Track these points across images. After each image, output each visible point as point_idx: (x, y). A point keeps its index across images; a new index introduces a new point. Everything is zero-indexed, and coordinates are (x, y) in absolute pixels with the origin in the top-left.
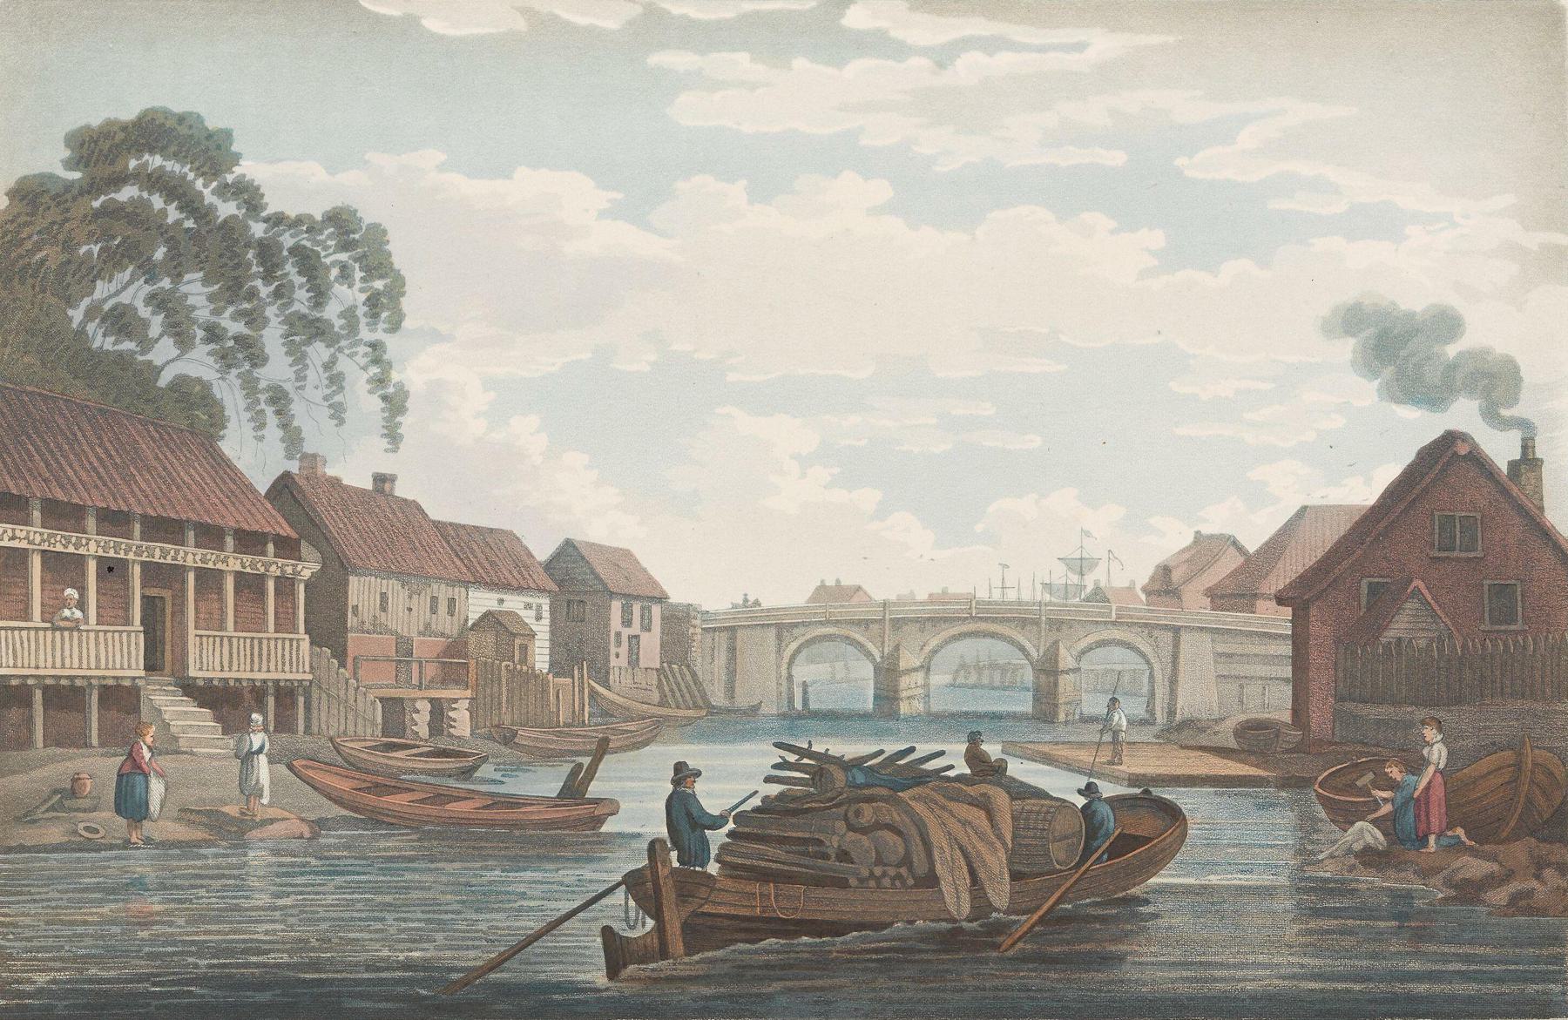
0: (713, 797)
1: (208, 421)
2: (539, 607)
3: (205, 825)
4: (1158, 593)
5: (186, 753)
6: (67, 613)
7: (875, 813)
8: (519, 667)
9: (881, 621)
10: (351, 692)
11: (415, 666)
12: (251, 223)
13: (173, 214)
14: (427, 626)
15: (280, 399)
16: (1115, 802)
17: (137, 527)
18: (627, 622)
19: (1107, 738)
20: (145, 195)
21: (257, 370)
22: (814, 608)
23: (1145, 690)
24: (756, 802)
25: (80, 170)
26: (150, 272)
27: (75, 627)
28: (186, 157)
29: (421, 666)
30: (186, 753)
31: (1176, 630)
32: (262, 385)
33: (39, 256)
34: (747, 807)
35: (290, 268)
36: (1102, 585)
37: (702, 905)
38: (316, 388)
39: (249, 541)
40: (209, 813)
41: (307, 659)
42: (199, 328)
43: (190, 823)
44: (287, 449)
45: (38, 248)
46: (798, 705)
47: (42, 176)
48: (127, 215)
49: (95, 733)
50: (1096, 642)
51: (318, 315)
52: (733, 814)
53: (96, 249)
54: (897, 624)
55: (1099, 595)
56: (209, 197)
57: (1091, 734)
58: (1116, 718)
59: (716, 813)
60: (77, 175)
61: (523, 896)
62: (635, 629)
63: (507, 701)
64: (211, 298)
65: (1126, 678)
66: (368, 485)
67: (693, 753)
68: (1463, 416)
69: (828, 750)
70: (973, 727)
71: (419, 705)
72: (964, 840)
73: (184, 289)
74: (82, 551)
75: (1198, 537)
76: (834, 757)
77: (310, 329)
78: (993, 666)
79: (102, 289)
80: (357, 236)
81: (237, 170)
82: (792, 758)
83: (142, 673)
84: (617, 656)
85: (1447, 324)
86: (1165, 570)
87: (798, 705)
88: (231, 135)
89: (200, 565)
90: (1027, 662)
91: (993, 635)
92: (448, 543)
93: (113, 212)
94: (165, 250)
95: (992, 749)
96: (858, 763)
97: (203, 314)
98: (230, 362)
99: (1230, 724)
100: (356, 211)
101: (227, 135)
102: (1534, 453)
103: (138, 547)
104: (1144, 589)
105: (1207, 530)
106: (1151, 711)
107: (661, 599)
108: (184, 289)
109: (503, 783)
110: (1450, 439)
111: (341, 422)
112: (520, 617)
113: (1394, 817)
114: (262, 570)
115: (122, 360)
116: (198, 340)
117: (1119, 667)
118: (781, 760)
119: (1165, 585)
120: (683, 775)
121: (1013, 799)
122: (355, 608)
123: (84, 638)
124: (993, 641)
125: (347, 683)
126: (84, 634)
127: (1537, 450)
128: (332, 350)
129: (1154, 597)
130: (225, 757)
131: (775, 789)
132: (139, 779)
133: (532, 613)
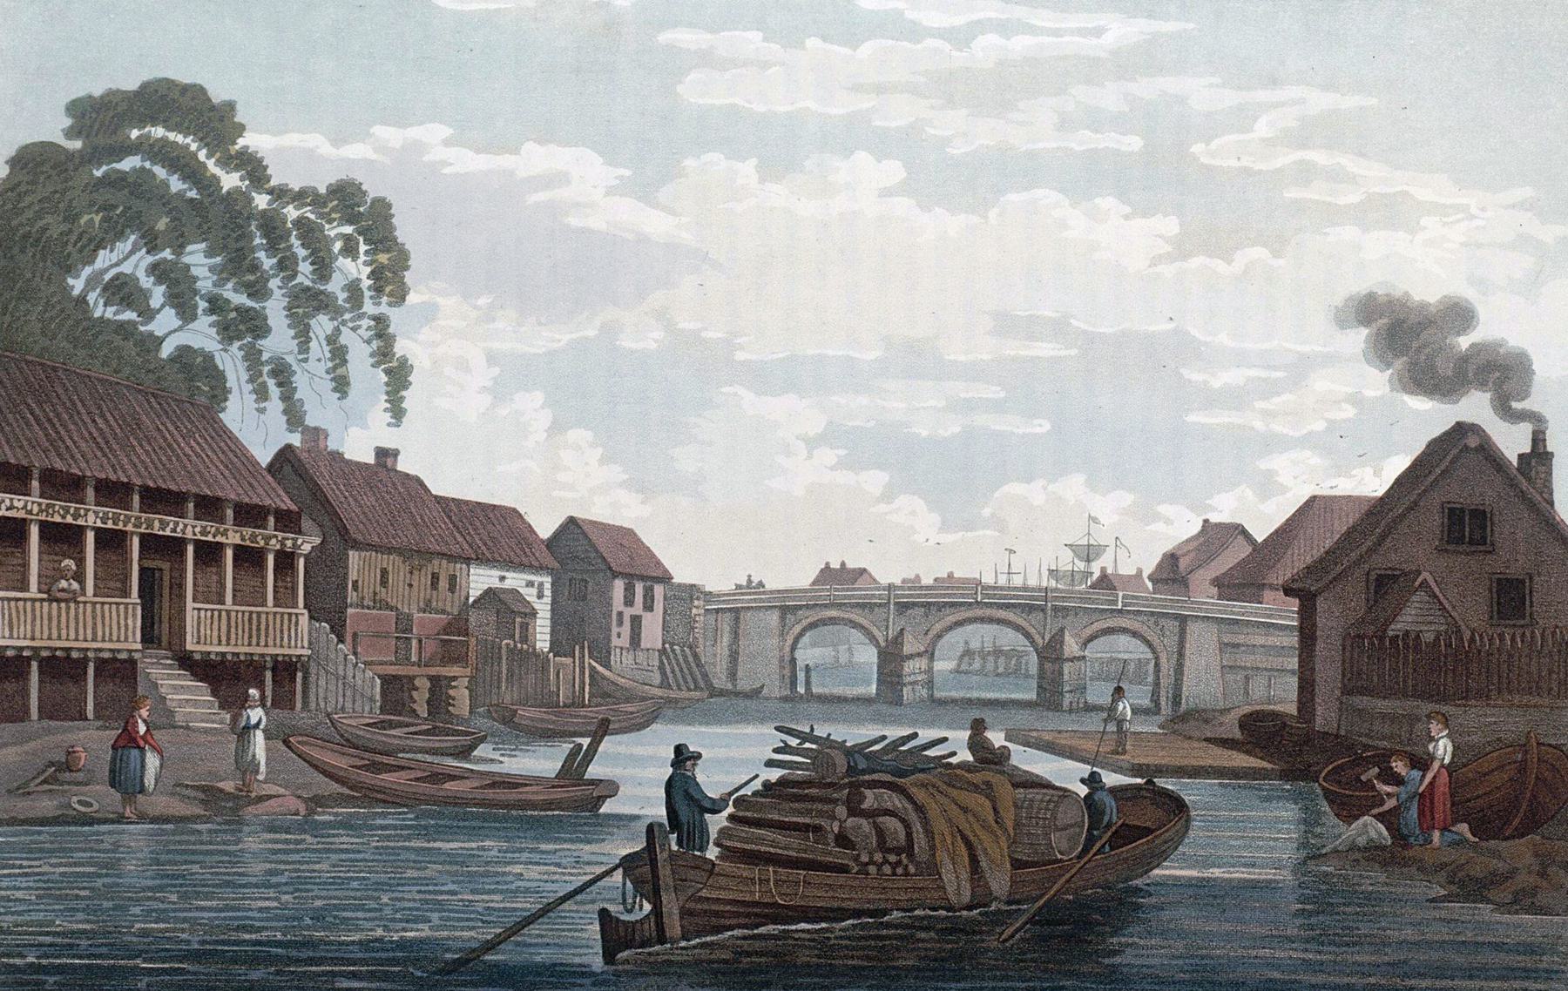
0: (712, 780)
2: (541, 585)
4: (1166, 581)
6: (63, 584)
8: (519, 645)
10: (350, 666)
11: (414, 643)
13: (176, 184)
14: (428, 602)
17: (136, 498)
18: (629, 602)
19: (1112, 727)
20: (147, 165)
23: (1150, 679)
24: (757, 785)
26: (152, 243)
30: (182, 727)
31: (1183, 620)
32: (265, 356)
33: (41, 223)
34: (747, 791)
36: (1109, 571)
38: (319, 360)
39: (249, 515)
42: (202, 298)
51: (322, 288)
53: (98, 219)
54: (903, 607)
56: (212, 167)
57: (1094, 723)
58: (1121, 707)
60: (77, 145)
62: (638, 608)
64: (212, 269)
65: (1132, 667)
66: (370, 459)
67: (694, 736)
68: (1476, 407)
69: (829, 735)
73: (186, 260)
74: (80, 522)
79: (104, 258)
81: (241, 142)
83: (139, 646)
84: (619, 635)
86: (1171, 559)
89: (199, 537)
91: (1000, 621)
92: (450, 518)
93: (117, 181)
95: (996, 738)
96: (859, 749)
97: (205, 284)
102: (1545, 447)
104: (1150, 578)
106: (1155, 700)
107: (665, 578)
110: (1461, 429)
114: (262, 543)
115: (125, 329)
116: (200, 311)
119: (1172, 572)
120: (683, 757)
123: (81, 610)
125: (345, 659)
128: (336, 323)
131: (774, 775)
133: (534, 591)
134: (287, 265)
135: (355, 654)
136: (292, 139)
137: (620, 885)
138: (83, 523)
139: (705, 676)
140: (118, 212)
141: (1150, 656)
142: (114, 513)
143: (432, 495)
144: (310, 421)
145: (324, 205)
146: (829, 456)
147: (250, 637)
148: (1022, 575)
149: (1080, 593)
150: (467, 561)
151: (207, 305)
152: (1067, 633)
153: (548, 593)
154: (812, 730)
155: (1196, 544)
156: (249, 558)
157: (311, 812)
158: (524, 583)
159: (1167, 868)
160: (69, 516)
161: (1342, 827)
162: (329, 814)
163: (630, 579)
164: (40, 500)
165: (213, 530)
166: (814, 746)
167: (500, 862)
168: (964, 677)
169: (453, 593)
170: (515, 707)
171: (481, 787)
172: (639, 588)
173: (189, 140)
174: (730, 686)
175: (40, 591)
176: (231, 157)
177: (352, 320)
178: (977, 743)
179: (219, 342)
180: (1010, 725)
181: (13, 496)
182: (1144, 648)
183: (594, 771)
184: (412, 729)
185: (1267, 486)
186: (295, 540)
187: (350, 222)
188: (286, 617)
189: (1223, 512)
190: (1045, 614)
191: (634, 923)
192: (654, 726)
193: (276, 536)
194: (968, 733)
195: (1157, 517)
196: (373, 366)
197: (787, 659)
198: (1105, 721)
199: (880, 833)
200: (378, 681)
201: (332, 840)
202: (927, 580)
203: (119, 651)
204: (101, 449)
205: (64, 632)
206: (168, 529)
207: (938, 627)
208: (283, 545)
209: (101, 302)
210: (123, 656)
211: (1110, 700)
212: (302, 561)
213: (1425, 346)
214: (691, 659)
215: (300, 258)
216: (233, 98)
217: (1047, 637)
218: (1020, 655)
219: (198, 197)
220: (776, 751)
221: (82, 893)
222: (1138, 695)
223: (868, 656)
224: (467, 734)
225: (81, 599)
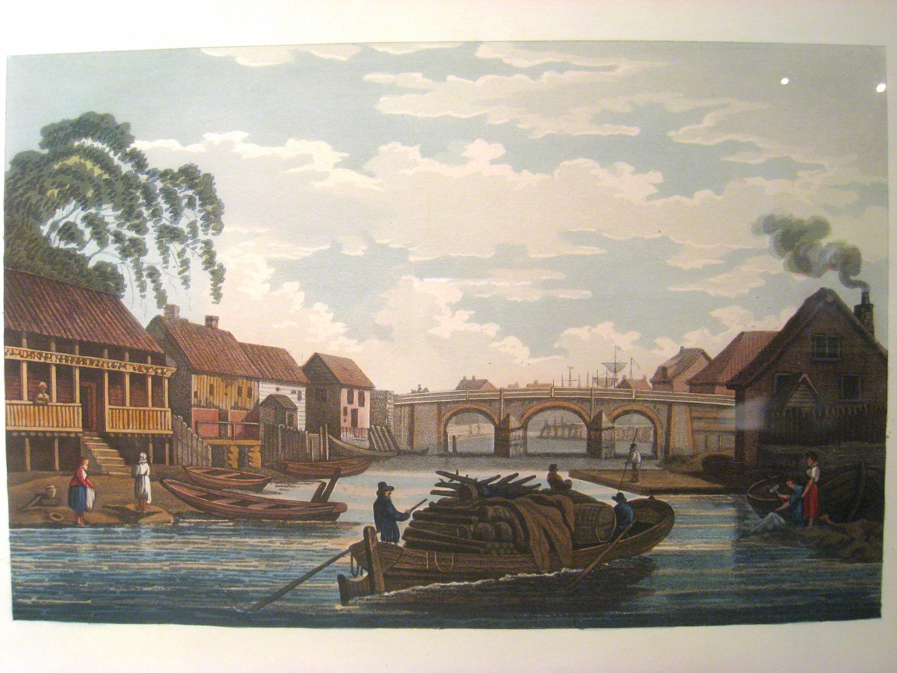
0: (402, 502)
1: (114, 287)
2: (300, 392)
3: (118, 515)
4: (659, 383)
5: (104, 475)
6: (41, 395)
7: (495, 511)
8: (288, 427)
9: (499, 400)
10: (195, 441)
11: (229, 427)
12: (139, 175)
13: (97, 171)
14: (236, 403)
15: (154, 274)
16: (635, 504)
17: (77, 347)
18: (350, 401)
19: (630, 467)
20: (83, 161)
21: (142, 258)
22: (459, 393)
23: (651, 439)
24: (426, 506)
25: (48, 148)
26: (85, 203)
27: (45, 403)
28: (104, 139)
29: (232, 426)
30: (104, 475)
31: (670, 405)
32: (145, 266)
33: (26, 196)
34: (421, 508)
35: (161, 200)
36: (627, 378)
37: (395, 564)
38: (174, 267)
39: (139, 356)
40: (117, 509)
41: (170, 423)
42: (111, 234)
43: (109, 514)
44: (158, 302)
45: (25, 192)
46: (450, 449)
47: (28, 152)
48: (74, 172)
49: (57, 463)
50: (624, 411)
51: (176, 226)
52: (412, 512)
53: (56, 192)
54: (508, 401)
55: (625, 384)
56: (117, 161)
57: (620, 465)
58: (635, 456)
59: (403, 512)
60: (46, 151)
61: (293, 558)
62: (356, 404)
63: (282, 447)
64: (117, 218)
65: (640, 433)
66: (203, 323)
67: (390, 476)
68: (831, 280)
69: (467, 475)
70: (552, 462)
71: (232, 449)
72: (547, 527)
73: (103, 213)
74: (48, 361)
75: (683, 351)
76: (472, 479)
77: (169, 234)
78: (564, 426)
79: (59, 214)
80: (197, 181)
81: (132, 146)
82: (447, 480)
83: (81, 430)
84: (345, 421)
85: (821, 227)
86: (663, 370)
87: (450, 449)
88: (129, 126)
89: (111, 369)
90: (583, 423)
91: (564, 408)
92: (248, 355)
93: (64, 171)
94: (93, 191)
95: (564, 476)
96: (485, 483)
97: (113, 226)
98: (128, 253)
99: (701, 457)
100: (197, 166)
101: (127, 126)
102: (869, 301)
103: (78, 359)
104: (651, 381)
105: (688, 345)
106: (655, 451)
107: (370, 388)
108: (103, 213)
109: (280, 494)
110: (823, 294)
111: (188, 287)
112: (289, 399)
113: (791, 509)
114: (145, 371)
115: (69, 254)
116: (110, 242)
117: (637, 427)
118: (440, 481)
119: (663, 378)
120: (384, 489)
121: (575, 503)
122: (196, 393)
123: (50, 410)
124: (564, 412)
125: (192, 436)
126: (50, 408)
127: (870, 299)
128: (183, 246)
129: (656, 385)
130: (127, 477)
131: (436, 499)
132: (81, 489)
133: (296, 396)
134: (156, 214)
135: (197, 433)
136: (159, 143)
137: (350, 561)
138: (50, 362)
139: (395, 443)
140: (67, 188)
141: (651, 425)
142: (66, 356)
143: (237, 342)
144: (170, 301)
145: (177, 179)
146: (463, 314)
147: (140, 425)
148: (577, 381)
149: (611, 390)
150: (258, 380)
151: (114, 238)
152: (603, 413)
153: (303, 397)
154: (457, 473)
155: (677, 361)
156: (138, 380)
157: (177, 522)
158: (290, 392)
159: (661, 546)
160: (36, 358)
161: (760, 520)
162: (186, 522)
163: (351, 388)
164: (28, 350)
165: (118, 365)
166: (459, 482)
167: (281, 550)
168: (544, 441)
169: (250, 398)
170: (287, 462)
171: (268, 508)
172: (356, 393)
173: (105, 146)
174: (409, 448)
175: (29, 400)
176: (127, 154)
177: (192, 244)
178: (553, 479)
179: (120, 259)
180: (572, 468)
181: (13, 348)
182: (648, 422)
183: (332, 498)
184: (229, 475)
185: (716, 326)
186: (163, 370)
187: (191, 188)
188: (159, 413)
189: (692, 340)
190: (591, 403)
191: (358, 583)
192: (366, 472)
193: (152, 367)
194: (547, 473)
195: (655, 345)
196: (204, 269)
197: (442, 433)
198: (626, 463)
199: (499, 531)
200: (210, 449)
201: (188, 537)
202: (522, 386)
203: (71, 432)
204: (58, 320)
205: (42, 422)
206: (94, 364)
207: (530, 411)
208: (156, 372)
209: (58, 238)
210: (73, 435)
211: (629, 451)
212: (166, 381)
213: (803, 244)
214: (386, 434)
215: (164, 209)
216: (128, 121)
217: (592, 417)
218: (576, 427)
219: (109, 178)
220: (437, 485)
221: (58, 565)
222: (645, 449)
223: (489, 430)
224: (261, 478)
225: (50, 404)
